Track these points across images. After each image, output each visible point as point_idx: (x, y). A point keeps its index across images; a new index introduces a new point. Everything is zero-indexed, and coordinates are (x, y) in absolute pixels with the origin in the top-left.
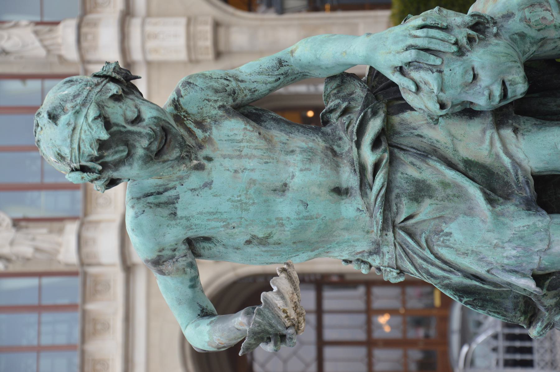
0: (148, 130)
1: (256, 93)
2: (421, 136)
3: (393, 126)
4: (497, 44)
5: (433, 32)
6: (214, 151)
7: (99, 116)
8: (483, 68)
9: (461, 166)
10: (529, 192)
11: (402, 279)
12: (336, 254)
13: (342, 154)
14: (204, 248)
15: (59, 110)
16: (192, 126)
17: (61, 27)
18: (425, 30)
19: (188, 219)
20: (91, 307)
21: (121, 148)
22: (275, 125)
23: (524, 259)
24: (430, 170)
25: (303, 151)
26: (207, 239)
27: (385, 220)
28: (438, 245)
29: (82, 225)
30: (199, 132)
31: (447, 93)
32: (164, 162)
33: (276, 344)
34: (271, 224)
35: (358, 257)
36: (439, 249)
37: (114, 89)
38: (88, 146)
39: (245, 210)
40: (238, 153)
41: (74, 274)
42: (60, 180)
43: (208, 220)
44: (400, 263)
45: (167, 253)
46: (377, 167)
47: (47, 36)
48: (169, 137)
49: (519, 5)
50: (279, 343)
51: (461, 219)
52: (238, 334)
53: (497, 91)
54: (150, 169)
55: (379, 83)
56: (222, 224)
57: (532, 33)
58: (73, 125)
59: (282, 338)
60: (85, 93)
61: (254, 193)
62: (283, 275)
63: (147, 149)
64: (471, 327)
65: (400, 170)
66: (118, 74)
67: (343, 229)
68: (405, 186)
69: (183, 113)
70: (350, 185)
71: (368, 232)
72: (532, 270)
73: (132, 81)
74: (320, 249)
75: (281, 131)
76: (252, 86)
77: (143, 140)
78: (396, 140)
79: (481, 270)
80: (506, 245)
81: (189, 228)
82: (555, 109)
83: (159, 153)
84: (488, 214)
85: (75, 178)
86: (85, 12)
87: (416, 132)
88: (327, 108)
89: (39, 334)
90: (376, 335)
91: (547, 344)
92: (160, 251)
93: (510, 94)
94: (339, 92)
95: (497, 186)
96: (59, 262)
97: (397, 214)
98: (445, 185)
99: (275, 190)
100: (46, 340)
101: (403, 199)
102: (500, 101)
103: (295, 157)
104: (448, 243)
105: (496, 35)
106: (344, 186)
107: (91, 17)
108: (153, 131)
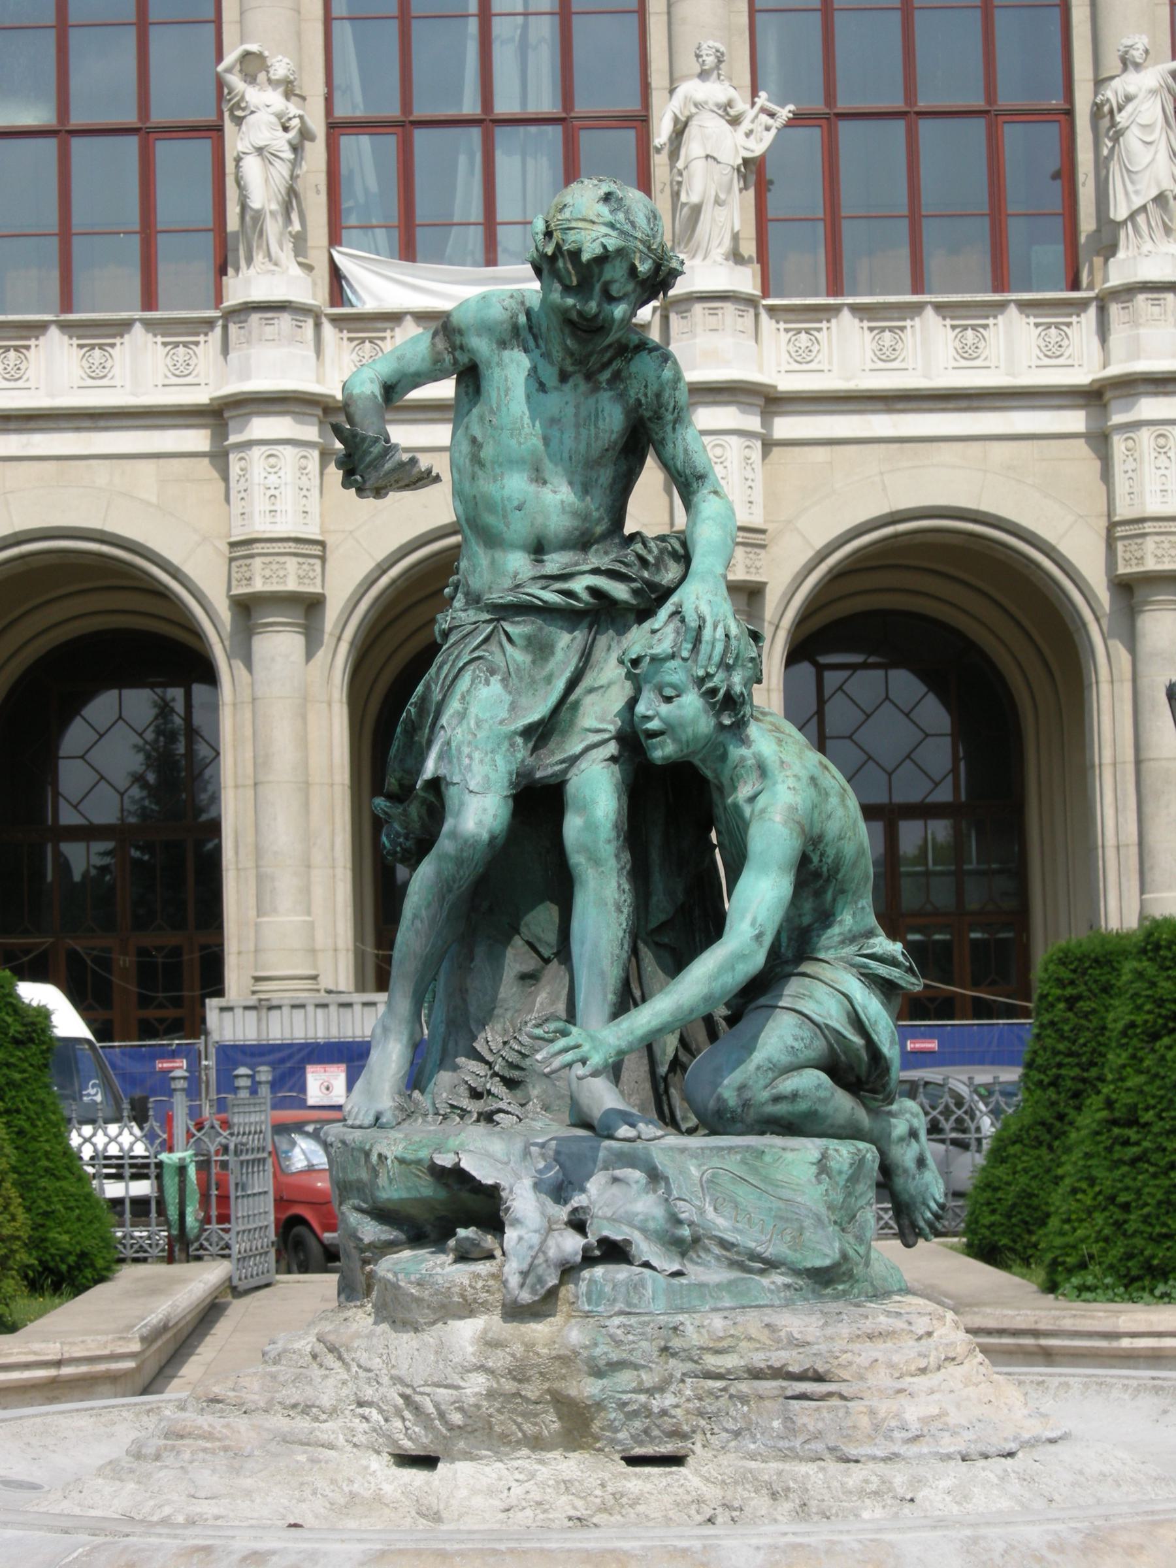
16: (615, 366)
28: (474, 671)
30: (606, 375)
39: (512, 434)
43: (498, 388)
53: (654, 725)
84: (512, 728)
94: (669, 553)
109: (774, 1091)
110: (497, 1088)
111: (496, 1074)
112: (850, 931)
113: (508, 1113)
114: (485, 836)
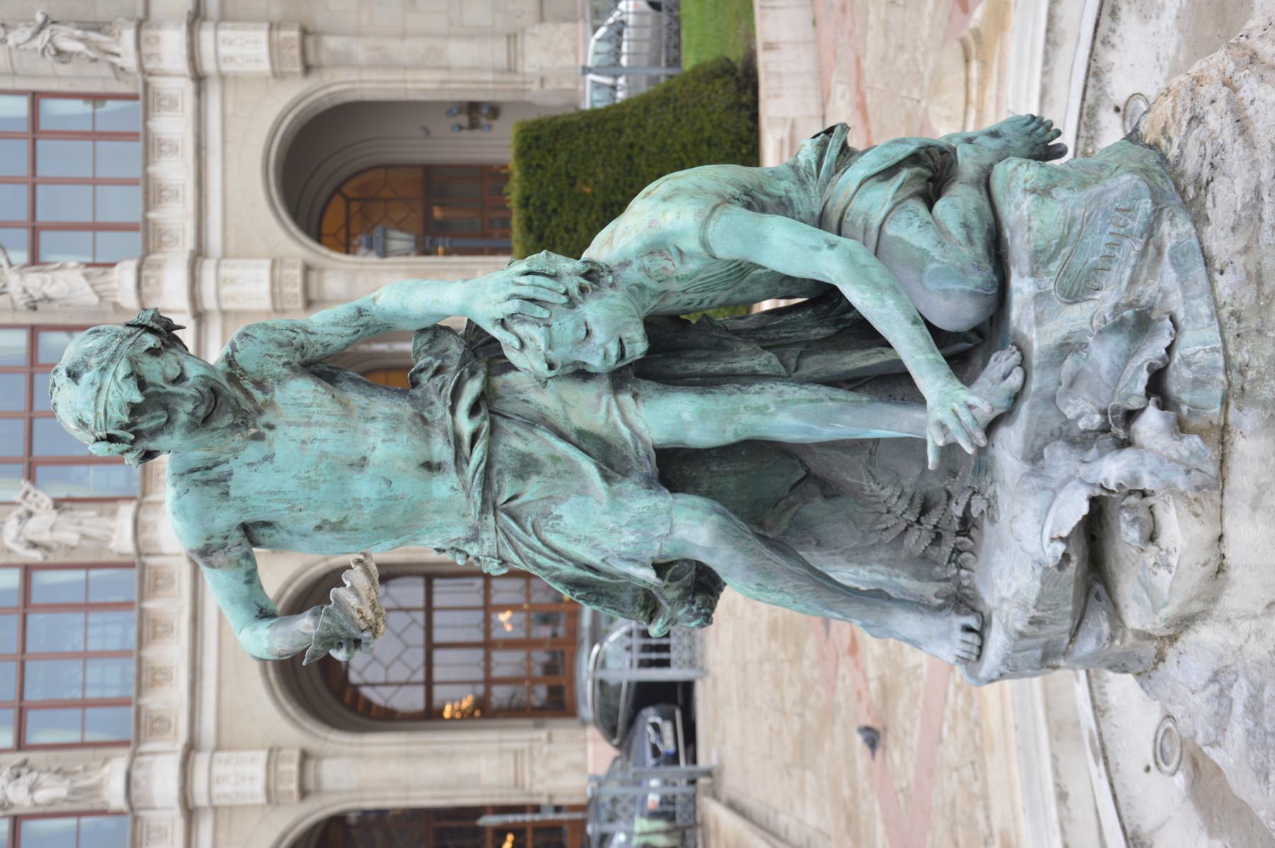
0: (193, 392)
1: (330, 348)
2: (528, 402)
3: (494, 389)
4: (613, 296)
5: (540, 280)
6: (277, 417)
7: (131, 374)
8: (597, 322)
9: (574, 437)
10: (650, 467)
11: (505, 571)
12: (426, 542)
13: (433, 422)
14: (263, 535)
15: (81, 367)
16: (250, 387)
17: (117, 269)
18: (530, 277)
19: (243, 499)
20: (149, 605)
21: (159, 413)
22: (353, 387)
23: (644, 545)
24: (538, 441)
25: (387, 418)
26: (267, 524)
27: (484, 501)
28: (546, 531)
29: (139, 506)
30: (258, 395)
31: (556, 350)
32: (214, 430)
33: (348, 651)
34: (346, 506)
35: (453, 545)
36: (548, 535)
37: (151, 340)
38: (116, 410)
39: (315, 489)
40: (306, 420)
41: (130, 565)
42: (78, 453)
43: (269, 501)
44: (502, 552)
45: (217, 541)
46: (474, 437)
47: (100, 280)
48: (219, 400)
49: (637, 252)
50: (352, 649)
51: (573, 499)
52: (304, 639)
53: (614, 350)
54: (196, 439)
55: (479, 338)
56: (286, 506)
57: (652, 284)
58: (98, 385)
59: (357, 643)
60: (114, 347)
61: (326, 468)
62: (358, 568)
63: (192, 414)
64: (603, 624)
65: (503, 441)
66: (157, 323)
67: (434, 512)
68: (509, 460)
69: (238, 372)
70: (443, 459)
71: (464, 515)
72: (652, 558)
73: (175, 332)
74: (407, 536)
75: (360, 393)
76: (326, 339)
77: (186, 403)
78: (497, 406)
79: (595, 560)
80: (623, 529)
81: (244, 510)
82: (679, 372)
83: (207, 420)
84: (604, 493)
85: (101, 449)
86: (147, 252)
87: (522, 397)
88: (416, 367)
89: (86, 638)
90: (496, 635)
91: (686, 641)
92: (208, 539)
93: (627, 354)
94: (430, 347)
95: (614, 461)
96: (111, 551)
97: (499, 493)
98: (555, 459)
99: (351, 465)
100: (94, 645)
101: (506, 476)
102: (617, 362)
103: (376, 424)
104: (557, 528)
105: (612, 285)
106: (436, 460)
107: (153, 257)
108: (200, 392)
109: (963, 243)
110: (932, 519)
111: (918, 521)
112: (794, 183)
113: (968, 505)
114: (715, 517)
